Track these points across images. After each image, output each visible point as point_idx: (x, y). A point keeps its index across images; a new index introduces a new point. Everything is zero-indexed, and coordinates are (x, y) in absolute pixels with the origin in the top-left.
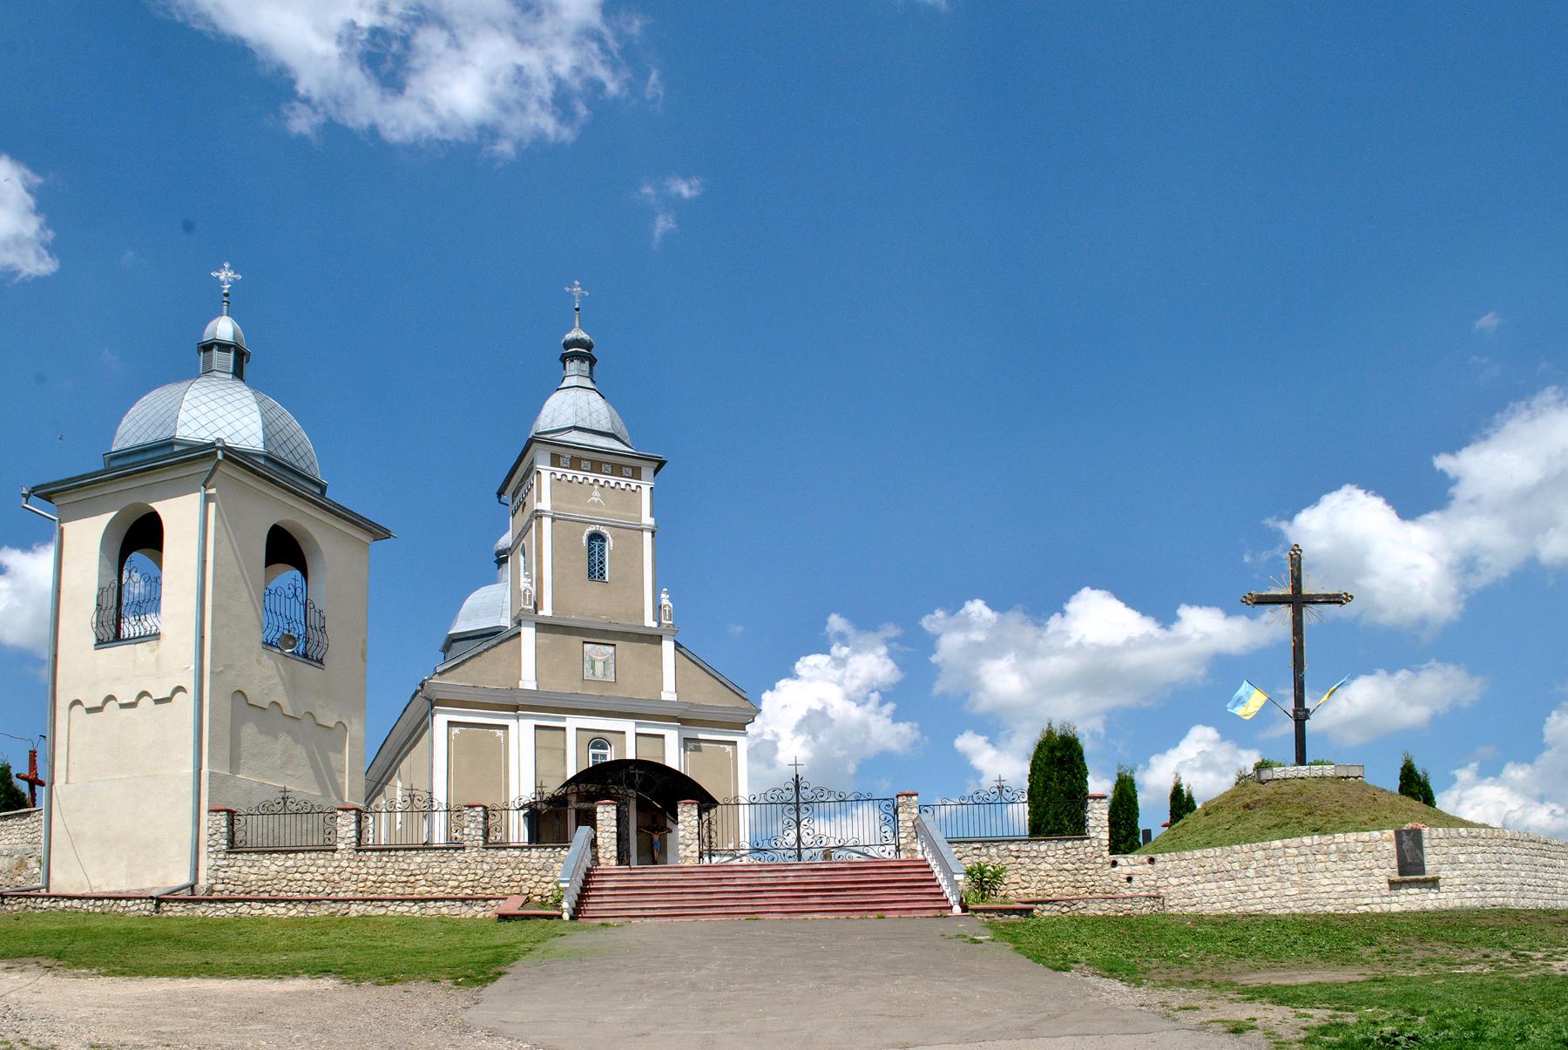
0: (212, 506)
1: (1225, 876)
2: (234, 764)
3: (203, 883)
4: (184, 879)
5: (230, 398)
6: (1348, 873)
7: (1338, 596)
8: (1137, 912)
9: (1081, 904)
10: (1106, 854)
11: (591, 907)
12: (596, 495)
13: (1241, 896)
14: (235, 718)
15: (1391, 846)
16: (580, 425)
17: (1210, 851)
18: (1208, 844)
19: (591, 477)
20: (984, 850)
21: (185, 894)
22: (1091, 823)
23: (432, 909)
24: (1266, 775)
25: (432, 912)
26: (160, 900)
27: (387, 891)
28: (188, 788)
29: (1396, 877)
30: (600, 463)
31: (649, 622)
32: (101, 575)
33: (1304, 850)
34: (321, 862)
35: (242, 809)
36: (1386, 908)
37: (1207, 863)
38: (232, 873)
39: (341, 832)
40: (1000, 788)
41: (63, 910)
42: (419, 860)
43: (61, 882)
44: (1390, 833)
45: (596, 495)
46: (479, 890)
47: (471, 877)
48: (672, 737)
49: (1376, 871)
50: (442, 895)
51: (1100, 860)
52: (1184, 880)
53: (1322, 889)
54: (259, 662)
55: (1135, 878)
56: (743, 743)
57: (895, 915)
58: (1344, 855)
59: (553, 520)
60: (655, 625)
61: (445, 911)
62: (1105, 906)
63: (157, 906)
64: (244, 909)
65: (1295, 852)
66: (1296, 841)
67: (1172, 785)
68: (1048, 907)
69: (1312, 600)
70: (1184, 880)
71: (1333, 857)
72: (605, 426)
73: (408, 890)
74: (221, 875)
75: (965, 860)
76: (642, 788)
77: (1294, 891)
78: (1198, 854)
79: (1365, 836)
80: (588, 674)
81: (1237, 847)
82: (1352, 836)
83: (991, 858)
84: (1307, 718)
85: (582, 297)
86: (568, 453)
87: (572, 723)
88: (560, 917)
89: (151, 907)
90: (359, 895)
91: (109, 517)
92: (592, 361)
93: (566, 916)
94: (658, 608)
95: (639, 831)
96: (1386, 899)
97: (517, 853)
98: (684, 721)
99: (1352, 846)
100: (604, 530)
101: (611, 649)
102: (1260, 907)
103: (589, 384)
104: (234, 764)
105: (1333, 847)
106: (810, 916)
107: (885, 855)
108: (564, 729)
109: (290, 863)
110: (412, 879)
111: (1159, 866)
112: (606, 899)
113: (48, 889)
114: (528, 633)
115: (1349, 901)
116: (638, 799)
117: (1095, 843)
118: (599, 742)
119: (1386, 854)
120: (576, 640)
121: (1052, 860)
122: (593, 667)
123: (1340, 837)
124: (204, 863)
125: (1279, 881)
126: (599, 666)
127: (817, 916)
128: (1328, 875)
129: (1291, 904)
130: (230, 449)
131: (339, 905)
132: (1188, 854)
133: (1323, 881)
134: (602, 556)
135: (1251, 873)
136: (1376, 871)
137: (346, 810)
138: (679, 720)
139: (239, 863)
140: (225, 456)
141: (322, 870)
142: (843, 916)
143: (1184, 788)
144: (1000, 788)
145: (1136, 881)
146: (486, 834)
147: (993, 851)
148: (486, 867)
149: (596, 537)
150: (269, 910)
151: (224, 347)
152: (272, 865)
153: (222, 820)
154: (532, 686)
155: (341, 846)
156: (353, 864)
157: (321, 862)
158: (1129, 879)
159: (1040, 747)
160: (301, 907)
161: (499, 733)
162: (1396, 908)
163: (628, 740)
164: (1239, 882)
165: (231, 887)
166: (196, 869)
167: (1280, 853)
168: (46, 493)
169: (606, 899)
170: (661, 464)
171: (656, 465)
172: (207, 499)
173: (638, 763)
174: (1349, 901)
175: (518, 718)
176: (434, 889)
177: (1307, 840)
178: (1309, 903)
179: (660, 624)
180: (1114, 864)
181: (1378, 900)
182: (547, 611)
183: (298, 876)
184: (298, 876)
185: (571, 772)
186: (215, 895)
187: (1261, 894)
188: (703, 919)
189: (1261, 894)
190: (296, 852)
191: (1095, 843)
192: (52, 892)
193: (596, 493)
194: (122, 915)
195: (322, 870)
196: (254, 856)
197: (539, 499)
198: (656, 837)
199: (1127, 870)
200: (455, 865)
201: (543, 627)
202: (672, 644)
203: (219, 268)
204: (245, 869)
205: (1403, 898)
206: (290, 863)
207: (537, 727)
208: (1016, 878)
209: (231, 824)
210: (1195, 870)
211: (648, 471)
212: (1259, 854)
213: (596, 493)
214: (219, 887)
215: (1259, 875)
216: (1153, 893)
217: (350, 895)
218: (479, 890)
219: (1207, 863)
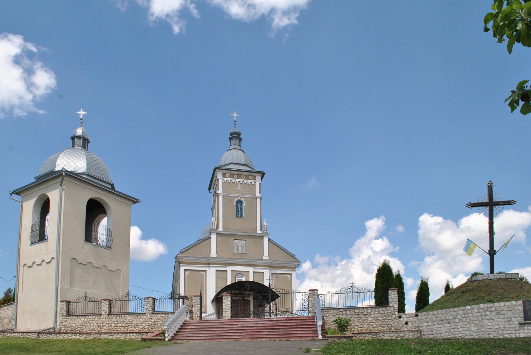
0: (64, 193)
1: (446, 322)
2: (71, 284)
3: (58, 327)
4: (52, 325)
5: (76, 155)
6: (500, 320)
7: (510, 201)
8: (406, 337)
9: (381, 334)
10: (397, 313)
11: (180, 336)
12: (239, 187)
13: (452, 331)
14: (71, 267)
15: (521, 308)
16: (234, 162)
17: (440, 311)
18: (442, 308)
19: (237, 181)
20: (344, 312)
21: (52, 331)
22: (390, 300)
23: (128, 336)
24: (475, 278)
25: (128, 337)
26: (39, 333)
27: (119, 330)
28: (54, 293)
29: (523, 321)
30: (241, 175)
32: (33, 220)
33: (480, 310)
34: (96, 319)
35: (72, 301)
36: (517, 335)
37: (439, 316)
38: (67, 323)
39: (103, 308)
40: (352, 287)
41: (13, 337)
42: (129, 318)
43: (21, 327)
44: (520, 302)
45: (239, 187)
46: (150, 329)
47: (147, 324)
48: (267, 273)
49: (513, 319)
50: (137, 331)
51: (394, 316)
52: (429, 324)
53: (488, 327)
54: (83, 248)
55: (409, 323)
56: (294, 273)
57: (294, 339)
58: (498, 312)
59: (223, 196)
60: (261, 232)
61: (133, 337)
62: (392, 335)
63: (38, 335)
64: (66, 336)
65: (476, 311)
66: (477, 306)
67: (445, 284)
68: (367, 335)
69: (498, 204)
70: (429, 324)
71: (494, 313)
72: (243, 162)
73: (126, 329)
74: (64, 324)
75: (337, 316)
77: (476, 328)
78: (435, 312)
79: (509, 303)
80: (236, 251)
81: (452, 309)
82: (502, 304)
83: (347, 315)
84: (495, 254)
85: (237, 117)
86: (228, 172)
87: (229, 269)
88: (164, 340)
89: (36, 336)
90: (109, 331)
91: (36, 199)
92: (240, 139)
93: (167, 339)
94: (262, 226)
95: (254, 307)
96: (518, 332)
97: (164, 315)
98: (271, 267)
99: (502, 308)
100: (242, 199)
101: (244, 242)
102: (461, 335)
103: (238, 147)
104: (71, 284)
105: (494, 309)
106: (259, 340)
107: (304, 315)
108: (226, 271)
109: (86, 320)
110: (127, 325)
111: (420, 318)
112: (187, 333)
113: (16, 328)
114: (214, 237)
115: (500, 332)
117: (392, 309)
118: (240, 273)
119: (518, 311)
120: (231, 239)
121: (373, 316)
122: (238, 248)
123: (497, 304)
124: (59, 320)
125: (469, 324)
126: (240, 248)
127: (264, 339)
128: (491, 321)
129: (474, 334)
130: (67, 171)
131: (97, 335)
132: (431, 313)
133: (489, 324)
134: (242, 208)
135: (457, 320)
136: (513, 319)
137: (105, 300)
138: (270, 267)
139: (70, 320)
140: (66, 174)
141: (97, 322)
142: (272, 340)
143: (450, 285)
144: (352, 287)
145: (410, 324)
146: (154, 309)
147: (348, 312)
148: (153, 321)
149: (239, 202)
150: (74, 337)
151: (79, 138)
152: (80, 320)
153: (64, 305)
154: (215, 256)
155: (103, 313)
156: (107, 320)
157: (96, 319)
158: (407, 323)
160: (84, 336)
161: (203, 273)
162: (522, 335)
164: (452, 324)
165: (67, 328)
166: (56, 322)
167: (470, 312)
168: (18, 192)
169: (187, 333)
170: (263, 174)
171: (261, 175)
172: (62, 190)
174: (500, 332)
175: (210, 267)
176: (135, 329)
177: (482, 306)
178: (482, 333)
180: (400, 317)
181: (514, 332)
182: (221, 229)
183: (89, 324)
184: (89, 324)
185: (229, 283)
186: (62, 331)
187: (461, 329)
188: (217, 341)
189: (461, 329)
190: (122, 314)
191: (392, 309)
192: (17, 331)
193: (239, 186)
194: (28, 338)
195: (97, 322)
196: (75, 317)
197: (218, 189)
199: (406, 320)
200: (142, 320)
201: (219, 235)
202: (267, 239)
203: (79, 110)
204: (71, 322)
205: (526, 331)
206: (86, 320)
207: (216, 270)
208: (358, 323)
209: (110, 305)
210: (434, 319)
211: (258, 178)
212: (461, 312)
213: (239, 186)
214: (63, 328)
215: (460, 321)
216: (417, 329)
217: (106, 331)
218: (150, 329)
219: (439, 316)
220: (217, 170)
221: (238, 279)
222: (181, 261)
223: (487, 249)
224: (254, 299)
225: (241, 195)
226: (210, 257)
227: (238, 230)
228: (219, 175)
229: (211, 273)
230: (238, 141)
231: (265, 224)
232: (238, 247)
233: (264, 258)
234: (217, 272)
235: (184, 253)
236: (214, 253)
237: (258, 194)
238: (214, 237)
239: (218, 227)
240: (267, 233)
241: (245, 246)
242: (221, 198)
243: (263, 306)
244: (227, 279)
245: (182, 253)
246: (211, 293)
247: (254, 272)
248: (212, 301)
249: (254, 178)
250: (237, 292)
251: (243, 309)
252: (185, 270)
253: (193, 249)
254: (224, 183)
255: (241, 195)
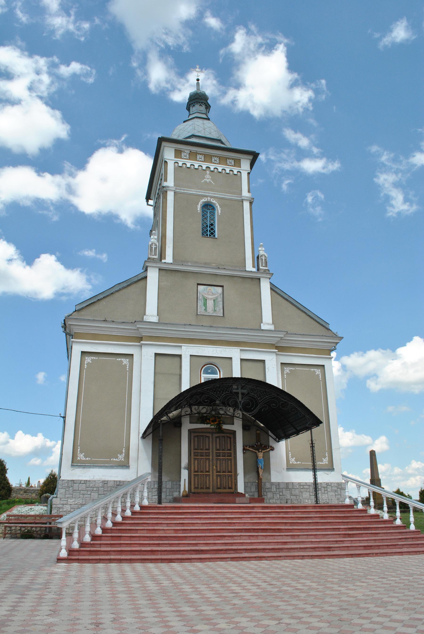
12: (208, 178)
31: (249, 267)
45: (208, 178)
60: (254, 270)
76: (246, 408)
80: (201, 310)
87: (187, 351)
92: (208, 107)
94: (257, 259)
98: (281, 349)
101: (220, 290)
108: (180, 356)
114: (153, 276)
116: (244, 419)
118: (210, 363)
120: (192, 282)
122: (205, 304)
126: (210, 303)
134: (213, 219)
138: (277, 348)
159: (33, 264)
163: (235, 363)
171: (251, 157)
173: (242, 381)
179: (258, 269)
182: (169, 258)
185: (185, 386)
197: (166, 180)
198: (260, 455)
202: (268, 286)
207: (156, 354)
211: (245, 165)
213: (208, 176)
220: (164, 144)
221: (204, 378)
222: (76, 330)
223: (186, 324)
224: (245, 428)
225: (211, 194)
226: (142, 321)
227: (206, 264)
228: (168, 154)
229: (144, 360)
230: (203, 108)
231: (262, 253)
232: (205, 300)
233: (263, 327)
234: (158, 358)
235: (82, 313)
236: (151, 313)
237: (245, 193)
238: (153, 276)
239: (162, 256)
240: (266, 272)
241: (220, 299)
242: (170, 196)
243: (267, 448)
244: (180, 376)
245: (79, 310)
246: (143, 413)
247: (242, 360)
248: (144, 436)
249: (237, 163)
250: (203, 410)
251: (218, 455)
252: (83, 353)
253: (103, 302)
254: (178, 169)
255: (211, 194)
